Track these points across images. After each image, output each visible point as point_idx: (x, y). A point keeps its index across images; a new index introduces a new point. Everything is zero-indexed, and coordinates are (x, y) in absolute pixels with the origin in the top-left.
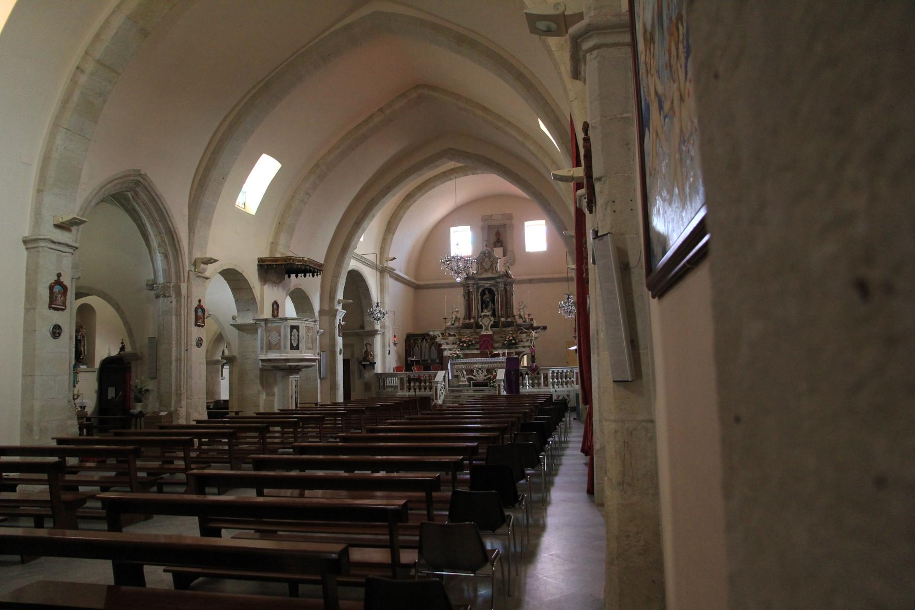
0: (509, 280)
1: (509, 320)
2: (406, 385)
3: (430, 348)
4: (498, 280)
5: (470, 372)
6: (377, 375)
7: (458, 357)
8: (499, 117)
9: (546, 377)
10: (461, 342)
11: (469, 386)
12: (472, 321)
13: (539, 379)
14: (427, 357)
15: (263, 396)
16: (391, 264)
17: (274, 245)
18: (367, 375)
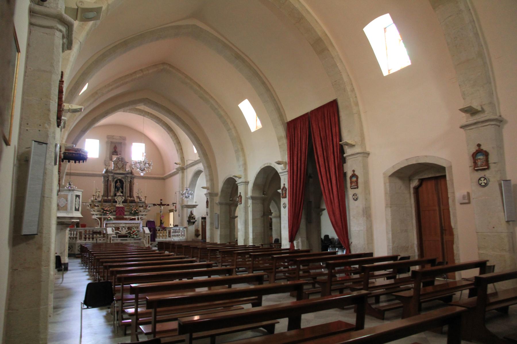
1: (132, 199)
2: (83, 236)
4: (128, 175)
5: (117, 229)
7: (111, 219)
8: (206, 93)
9: (170, 232)
12: (110, 198)
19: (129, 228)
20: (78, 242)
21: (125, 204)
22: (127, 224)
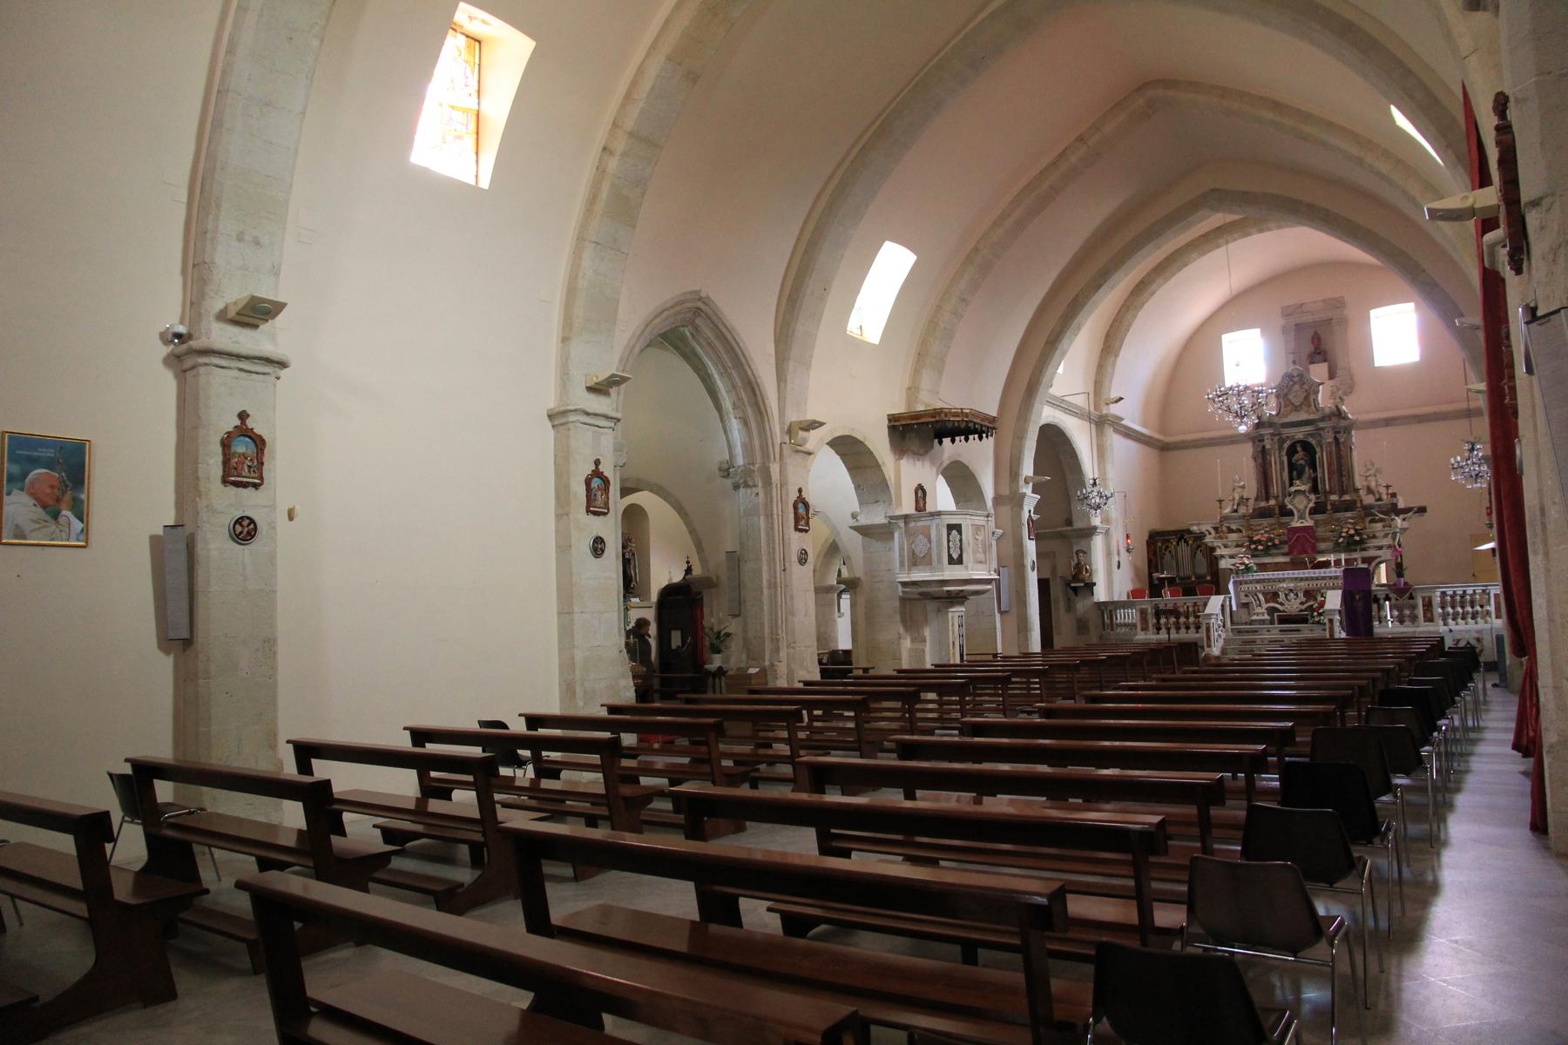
0: (1343, 423)
2: (1152, 621)
3: (1194, 555)
4: (1321, 425)
6: (1100, 605)
7: (1248, 569)
9: (1428, 605)
10: (1252, 542)
11: (1272, 622)
12: (1272, 502)
13: (1414, 607)
14: (1190, 573)
15: (907, 643)
16: (1114, 409)
17: (913, 391)
18: (1081, 605)
19: (1309, 594)
21: (1319, 517)
22: (1301, 579)
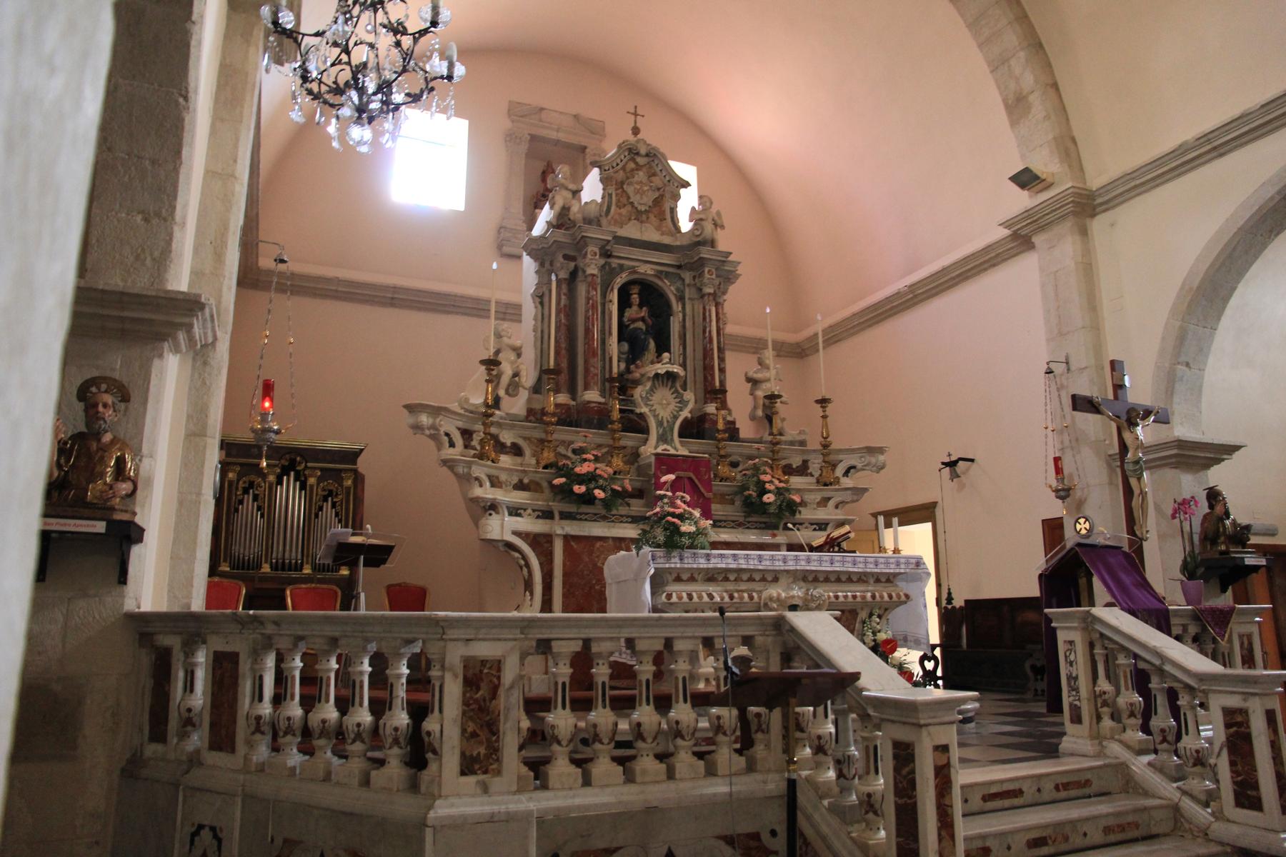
14: (293, 555)
20: (442, 810)
